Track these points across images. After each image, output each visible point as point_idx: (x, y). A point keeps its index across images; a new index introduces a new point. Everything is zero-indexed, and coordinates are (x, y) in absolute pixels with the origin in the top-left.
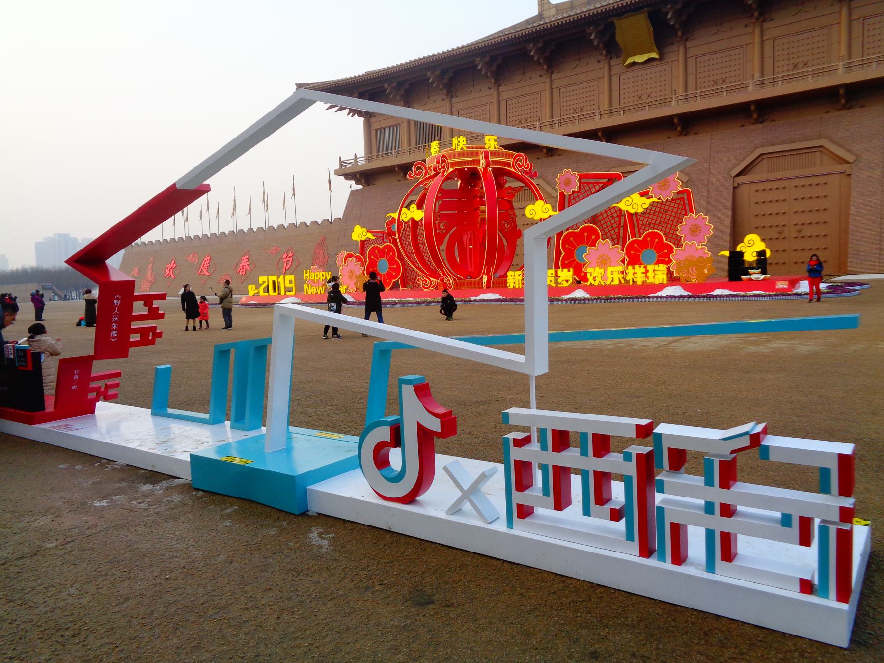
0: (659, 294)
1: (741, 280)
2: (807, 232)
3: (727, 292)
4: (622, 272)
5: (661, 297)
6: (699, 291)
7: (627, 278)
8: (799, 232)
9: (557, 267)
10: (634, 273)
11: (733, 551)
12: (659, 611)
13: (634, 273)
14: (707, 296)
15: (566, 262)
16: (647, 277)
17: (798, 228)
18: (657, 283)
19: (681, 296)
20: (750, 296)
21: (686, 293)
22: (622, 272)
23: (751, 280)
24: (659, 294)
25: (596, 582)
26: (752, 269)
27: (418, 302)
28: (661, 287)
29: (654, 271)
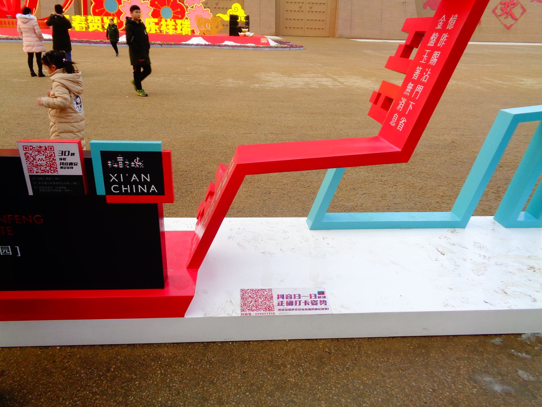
0: (188, 42)
1: (238, 35)
2: (315, 8)
3: (252, 45)
4: (157, 24)
5: (189, 45)
6: (214, 41)
7: (162, 29)
8: (300, 7)
9: (86, 13)
10: (167, 25)
11: (161, 230)
12: (293, 346)
13: (167, 25)
14: (219, 46)
15: (97, 11)
16: (176, 29)
17: (311, 5)
18: (184, 34)
19: (206, 45)
20: (248, 47)
21: (207, 43)
22: (157, 24)
23: (245, 35)
24: (188, 42)
25: (287, 338)
26: (243, 28)
27: (7, 39)
28: (188, 38)
29: (181, 24)
